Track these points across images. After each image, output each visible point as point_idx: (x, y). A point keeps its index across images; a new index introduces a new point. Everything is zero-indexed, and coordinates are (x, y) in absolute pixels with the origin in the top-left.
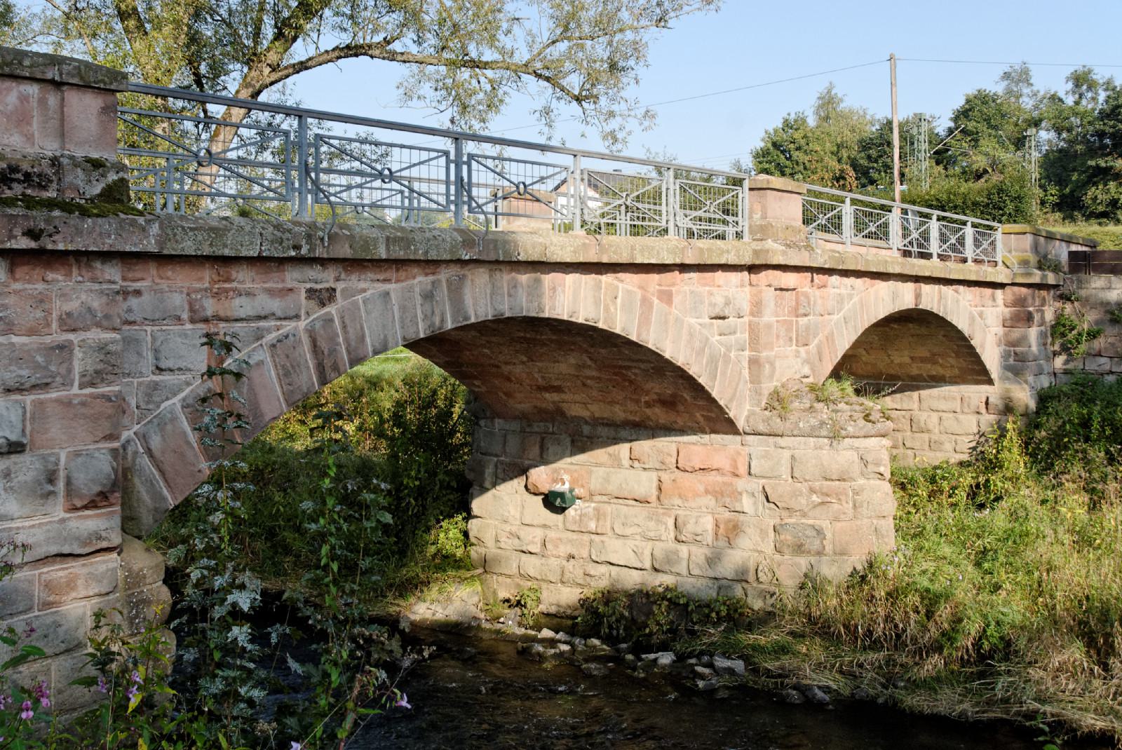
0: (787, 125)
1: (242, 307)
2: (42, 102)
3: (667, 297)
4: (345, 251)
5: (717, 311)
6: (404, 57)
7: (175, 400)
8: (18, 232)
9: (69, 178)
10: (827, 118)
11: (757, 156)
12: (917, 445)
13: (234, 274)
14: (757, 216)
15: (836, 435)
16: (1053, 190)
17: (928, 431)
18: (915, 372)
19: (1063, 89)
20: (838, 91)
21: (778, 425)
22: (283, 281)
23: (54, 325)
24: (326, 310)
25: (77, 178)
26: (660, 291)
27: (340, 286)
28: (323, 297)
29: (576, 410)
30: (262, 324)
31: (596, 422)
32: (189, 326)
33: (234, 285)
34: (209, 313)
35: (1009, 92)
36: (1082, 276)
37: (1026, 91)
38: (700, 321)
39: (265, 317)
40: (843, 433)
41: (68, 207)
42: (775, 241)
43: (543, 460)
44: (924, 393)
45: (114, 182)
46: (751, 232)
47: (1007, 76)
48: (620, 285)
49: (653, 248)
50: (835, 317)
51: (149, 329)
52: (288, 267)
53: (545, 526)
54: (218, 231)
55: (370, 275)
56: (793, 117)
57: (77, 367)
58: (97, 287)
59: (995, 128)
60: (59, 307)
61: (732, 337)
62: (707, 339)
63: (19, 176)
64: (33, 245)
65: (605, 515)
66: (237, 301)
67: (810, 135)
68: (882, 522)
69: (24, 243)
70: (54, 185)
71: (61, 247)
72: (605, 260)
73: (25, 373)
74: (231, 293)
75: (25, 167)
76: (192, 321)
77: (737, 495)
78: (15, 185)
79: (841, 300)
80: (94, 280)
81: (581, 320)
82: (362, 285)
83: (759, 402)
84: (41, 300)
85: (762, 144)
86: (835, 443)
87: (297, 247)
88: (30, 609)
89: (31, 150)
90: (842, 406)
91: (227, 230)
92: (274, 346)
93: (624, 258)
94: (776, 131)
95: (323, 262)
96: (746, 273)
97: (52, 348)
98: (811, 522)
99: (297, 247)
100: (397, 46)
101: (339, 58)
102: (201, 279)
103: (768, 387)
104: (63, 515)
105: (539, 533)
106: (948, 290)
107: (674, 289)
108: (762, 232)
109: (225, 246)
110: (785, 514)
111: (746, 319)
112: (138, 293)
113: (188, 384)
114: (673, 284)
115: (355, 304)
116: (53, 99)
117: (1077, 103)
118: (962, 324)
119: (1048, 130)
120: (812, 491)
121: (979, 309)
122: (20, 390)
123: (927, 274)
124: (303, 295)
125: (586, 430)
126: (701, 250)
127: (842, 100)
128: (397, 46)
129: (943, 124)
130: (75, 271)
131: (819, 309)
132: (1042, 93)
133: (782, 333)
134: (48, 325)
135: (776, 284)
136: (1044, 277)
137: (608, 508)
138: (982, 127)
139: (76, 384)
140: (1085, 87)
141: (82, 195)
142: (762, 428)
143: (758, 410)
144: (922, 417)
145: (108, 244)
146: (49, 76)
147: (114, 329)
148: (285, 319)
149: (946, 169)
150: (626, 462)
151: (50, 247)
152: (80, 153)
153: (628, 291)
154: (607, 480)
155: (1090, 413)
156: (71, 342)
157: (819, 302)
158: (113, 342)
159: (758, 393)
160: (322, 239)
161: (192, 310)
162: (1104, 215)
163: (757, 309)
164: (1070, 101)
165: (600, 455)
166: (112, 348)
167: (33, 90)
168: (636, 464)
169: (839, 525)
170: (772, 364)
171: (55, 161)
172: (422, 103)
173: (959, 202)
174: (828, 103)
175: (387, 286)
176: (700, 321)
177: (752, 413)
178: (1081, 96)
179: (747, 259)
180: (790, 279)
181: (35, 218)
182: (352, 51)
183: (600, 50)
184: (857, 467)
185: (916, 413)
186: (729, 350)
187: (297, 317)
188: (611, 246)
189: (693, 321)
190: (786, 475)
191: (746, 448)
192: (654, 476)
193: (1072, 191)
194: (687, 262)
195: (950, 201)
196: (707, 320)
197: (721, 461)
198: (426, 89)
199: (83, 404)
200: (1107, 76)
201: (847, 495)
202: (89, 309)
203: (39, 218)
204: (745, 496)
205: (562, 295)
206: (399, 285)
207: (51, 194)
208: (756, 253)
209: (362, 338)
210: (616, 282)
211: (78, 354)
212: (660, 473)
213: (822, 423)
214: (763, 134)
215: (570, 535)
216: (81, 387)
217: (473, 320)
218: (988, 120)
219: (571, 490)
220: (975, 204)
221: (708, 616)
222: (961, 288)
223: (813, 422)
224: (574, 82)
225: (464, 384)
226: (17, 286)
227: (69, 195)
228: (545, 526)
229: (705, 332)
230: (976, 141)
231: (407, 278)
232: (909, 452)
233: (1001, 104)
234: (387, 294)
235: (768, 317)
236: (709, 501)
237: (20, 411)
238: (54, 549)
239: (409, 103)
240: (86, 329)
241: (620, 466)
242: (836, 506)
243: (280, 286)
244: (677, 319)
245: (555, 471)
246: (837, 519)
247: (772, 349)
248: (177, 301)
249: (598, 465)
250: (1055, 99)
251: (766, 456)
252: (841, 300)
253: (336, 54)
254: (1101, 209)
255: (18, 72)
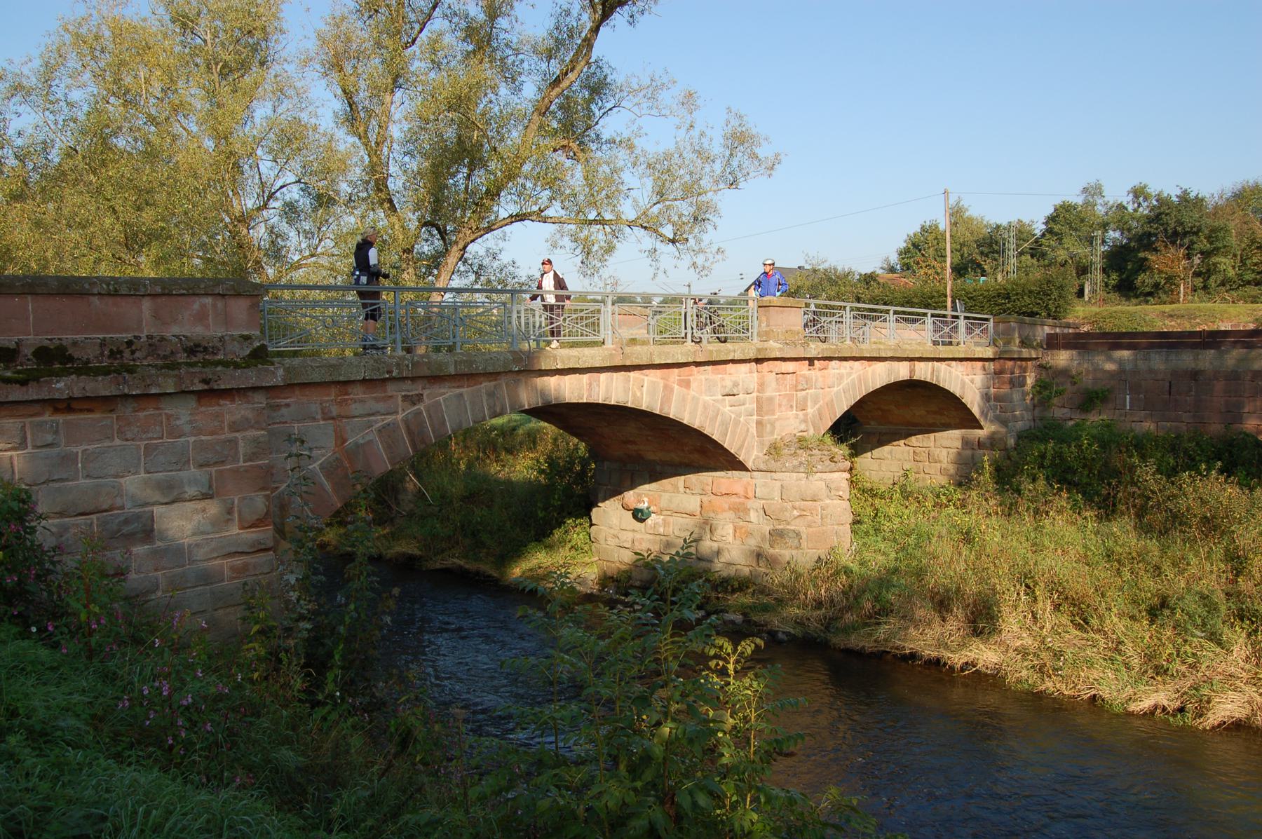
0: (923, 229)
1: (356, 409)
2: (214, 306)
3: (687, 384)
4: (427, 372)
5: (727, 391)
6: (553, 220)
10: (955, 224)
12: (932, 471)
13: (350, 390)
15: (810, 472)
17: (940, 462)
18: (931, 421)
19: (1127, 200)
20: (965, 203)
24: (417, 407)
25: (235, 347)
27: (426, 392)
28: (415, 399)
29: (650, 456)
30: (372, 418)
32: (322, 422)
33: (351, 396)
34: (334, 414)
35: (1087, 203)
36: (1055, 351)
37: (1099, 201)
39: (373, 414)
42: (776, 341)
43: (632, 487)
46: (759, 334)
47: (1085, 190)
48: (646, 378)
49: (669, 353)
51: (296, 425)
53: (634, 531)
54: (334, 367)
55: (447, 384)
56: (928, 224)
57: (241, 451)
58: (251, 406)
59: (1076, 230)
60: (228, 418)
62: (719, 410)
65: (669, 524)
66: (353, 406)
67: (939, 237)
68: (841, 527)
72: (628, 363)
73: (210, 456)
76: (324, 419)
77: (747, 511)
79: (841, 377)
80: (248, 402)
81: (613, 403)
83: (763, 449)
85: (905, 245)
86: (810, 478)
87: (389, 372)
89: (207, 333)
95: (413, 379)
96: (754, 364)
98: (793, 528)
99: (389, 372)
101: (512, 222)
102: (328, 395)
103: (769, 439)
104: (238, 531)
106: (942, 365)
107: (691, 378)
108: (765, 336)
109: (340, 375)
110: (776, 523)
111: (755, 395)
113: (323, 456)
115: (438, 403)
117: (1135, 210)
118: (955, 389)
119: (1114, 230)
120: (794, 508)
122: (208, 465)
124: (400, 399)
125: (658, 468)
126: (711, 352)
127: (967, 210)
129: (1039, 228)
130: (237, 399)
131: (819, 384)
132: (1111, 203)
133: (784, 402)
134: (222, 429)
135: (777, 370)
137: (671, 519)
138: (1066, 229)
139: (241, 460)
140: (1141, 199)
142: (762, 467)
143: (761, 455)
144: (936, 452)
145: (253, 381)
146: (217, 292)
148: (388, 414)
149: (1038, 260)
150: (682, 489)
151: (216, 387)
152: (236, 333)
154: (670, 501)
155: (1046, 449)
156: (236, 437)
157: (820, 379)
158: (263, 436)
159: (762, 443)
160: (408, 366)
163: (762, 386)
164: (1130, 208)
165: (666, 483)
166: (262, 439)
168: (688, 491)
171: (221, 339)
172: (563, 251)
173: (1020, 291)
174: (957, 215)
177: (757, 457)
178: (1139, 205)
179: (752, 355)
180: (790, 366)
182: (520, 217)
183: (686, 208)
184: (825, 491)
185: (933, 449)
186: (739, 415)
190: (777, 498)
192: (698, 498)
193: (1128, 277)
195: (1013, 289)
196: (721, 397)
197: (738, 488)
198: (566, 241)
199: (246, 471)
200: (1159, 190)
202: (247, 419)
205: (597, 389)
207: (220, 357)
210: (642, 377)
211: (241, 444)
213: (801, 463)
214: (905, 237)
219: (648, 508)
223: (795, 463)
224: (668, 231)
227: (229, 357)
228: (634, 531)
229: (718, 405)
230: (1061, 239)
231: (475, 384)
232: (927, 476)
233: (1080, 211)
234: (461, 395)
235: (769, 393)
236: (731, 514)
237: (208, 477)
238: (233, 550)
239: (555, 251)
241: (678, 492)
242: (810, 518)
245: (639, 495)
246: (809, 526)
247: (773, 414)
248: (315, 408)
249: (664, 491)
250: (1121, 207)
252: (841, 377)
254: (1148, 289)
255: (198, 292)
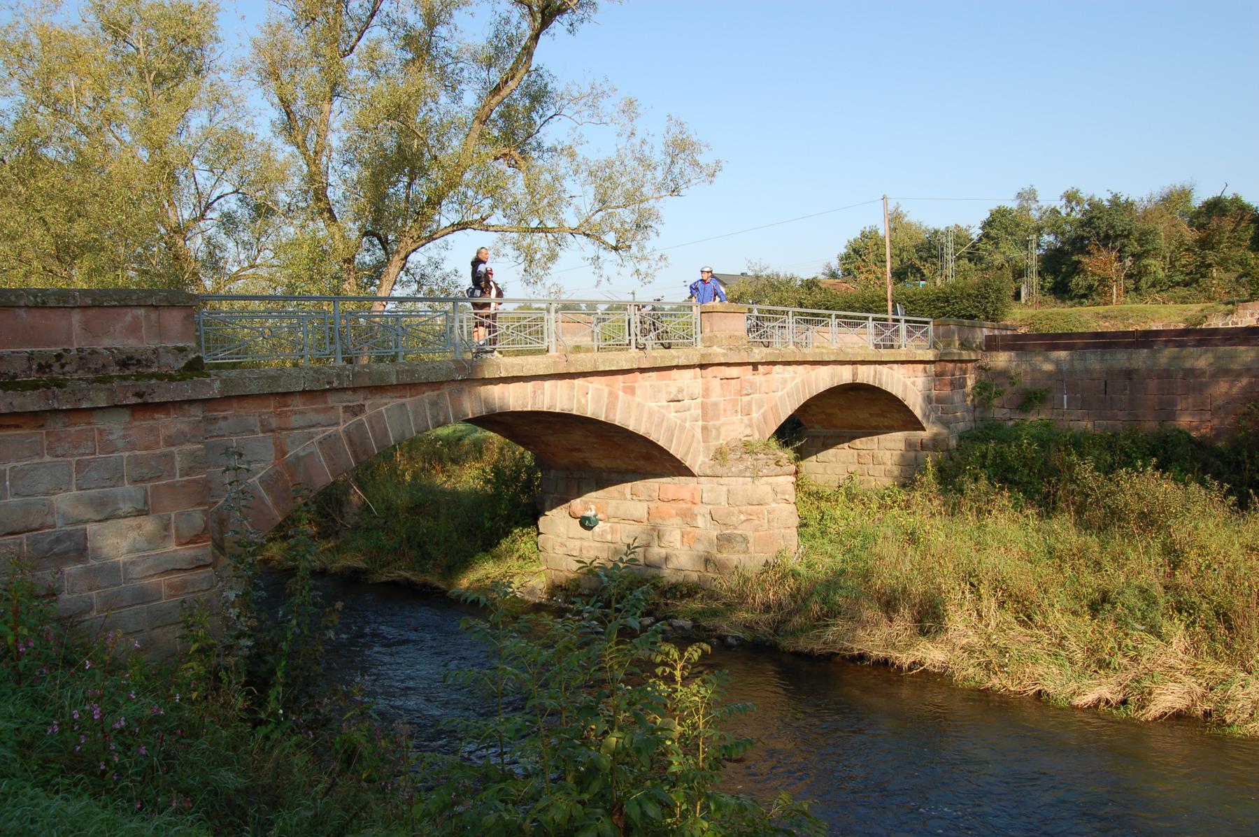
0: (863, 235)
1: (296, 420)
2: (147, 317)
4: (368, 383)
5: (672, 397)
6: (495, 229)
7: (255, 479)
8: (130, 394)
9: (163, 360)
11: (841, 259)
13: (289, 402)
14: (707, 330)
15: (756, 476)
16: (1049, 279)
17: (884, 464)
18: (874, 423)
19: (1060, 204)
21: (719, 470)
22: (326, 403)
23: (161, 443)
26: (624, 387)
27: (367, 403)
28: (357, 410)
29: (596, 463)
31: (611, 471)
32: (261, 435)
33: (291, 408)
34: (274, 426)
35: (1021, 208)
37: (1034, 206)
38: (659, 404)
39: (314, 426)
40: (760, 474)
41: (160, 377)
44: (882, 437)
45: (193, 359)
47: (1020, 195)
48: (590, 385)
49: (613, 360)
50: (779, 394)
51: (234, 438)
52: (329, 394)
54: (274, 379)
56: (868, 229)
57: (178, 466)
58: (187, 419)
59: (1011, 234)
60: (163, 432)
61: (688, 413)
63: (134, 362)
64: (139, 401)
65: (616, 531)
66: (293, 418)
69: (134, 400)
70: (156, 365)
71: (157, 400)
73: (145, 471)
74: (857, 305)
75: (137, 356)
76: (263, 432)
77: (694, 516)
78: (131, 367)
79: (784, 382)
81: (557, 411)
82: (385, 401)
83: (708, 454)
84: (152, 430)
85: (845, 251)
88: (160, 598)
90: (762, 456)
91: (280, 376)
92: (321, 442)
93: (589, 369)
94: (855, 240)
95: (354, 390)
96: (698, 369)
97: (161, 457)
98: (740, 532)
100: (489, 221)
102: (268, 407)
103: (714, 444)
104: (175, 548)
105: (578, 543)
107: (636, 385)
108: (709, 342)
109: (279, 386)
111: (699, 400)
112: (225, 418)
113: (263, 469)
114: (635, 382)
116: (153, 315)
117: (1068, 215)
120: (741, 512)
121: (912, 379)
122: (142, 481)
123: (860, 359)
124: (341, 410)
125: (605, 475)
126: (655, 358)
128: (489, 221)
129: (976, 233)
130: (172, 411)
131: (764, 389)
132: (1045, 207)
134: (158, 443)
136: (970, 355)
137: (618, 526)
138: (1002, 233)
139: (178, 475)
140: (1074, 203)
141: (172, 369)
142: (708, 472)
143: (707, 460)
146: (149, 303)
147: (199, 443)
148: (328, 426)
149: (976, 265)
151: (150, 401)
152: (170, 345)
153: (597, 389)
154: (617, 508)
158: (199, 449)
160: (348, 376)
161: (262, 425)
162: (1084, 296)
163: (706, 392)
165: (613, 490)
167: (141, 312)
168: (635, 497)
169: (758, 533)
170: (718, 430)
171: (155, 351)
172: (505, 259)
174: (896, 220)
175: (404, 400)
176: (659, 404)
178: (1072, 209)
179: (696, 361)
180: (734, 371)
181: (139, 386)
183: (628, 216)
184: (771, 495)
185: (876, 451)
187: (338, 424)
188: (576, 361)
189: (653, 404)
190: (724, 503)
191: (700, 486)
192: (645, 505)
193: (1063, 279)
194: (643, 366)
195: (952, 293)
196: (665, 403)
197: (685, 494)
198: (509, 249)
199: (182, 486)
201: (763, 514)
202: (183, 433)
203: (142, 385)
204: (699, 517)
206: (412, 399)
207: (154, 370)
208: (703, 355)
209: (386, 434)
210: (586, 384)
211: (178, 458)
212: (650, 503)
214: (846, 243)
215: (596, 544)
216: (181, 477)
217: (470, 416)
218: (1006, 228)
219: (595, 516)
220: (969, 295)
221: (675, 594)
222: (895, 366)
223: (741, 467)
224: (611, 238)
225: (529, 449)
226: (137, 423)
227: (164, 370)
229: (664, 411)
230: (997, 244)
231: (417, 394)
236: (678, 520)
237: (143, 492)
239: (498, 260)
240: (182, 444)
241: (625, 499)
242: (756, 522)
243: (323, 406)
244: (639, 404)
245: (586, 503)
246: (756, 530)
247: (718, 419)
248: (253, 421)
249: (611, 498)
250: (1055, 212)
251: (712, 490)
252: (784, 382)
253: (451, 229)
254: (1082, 292)
255: (130, 303)
